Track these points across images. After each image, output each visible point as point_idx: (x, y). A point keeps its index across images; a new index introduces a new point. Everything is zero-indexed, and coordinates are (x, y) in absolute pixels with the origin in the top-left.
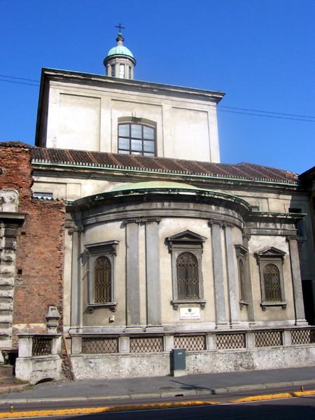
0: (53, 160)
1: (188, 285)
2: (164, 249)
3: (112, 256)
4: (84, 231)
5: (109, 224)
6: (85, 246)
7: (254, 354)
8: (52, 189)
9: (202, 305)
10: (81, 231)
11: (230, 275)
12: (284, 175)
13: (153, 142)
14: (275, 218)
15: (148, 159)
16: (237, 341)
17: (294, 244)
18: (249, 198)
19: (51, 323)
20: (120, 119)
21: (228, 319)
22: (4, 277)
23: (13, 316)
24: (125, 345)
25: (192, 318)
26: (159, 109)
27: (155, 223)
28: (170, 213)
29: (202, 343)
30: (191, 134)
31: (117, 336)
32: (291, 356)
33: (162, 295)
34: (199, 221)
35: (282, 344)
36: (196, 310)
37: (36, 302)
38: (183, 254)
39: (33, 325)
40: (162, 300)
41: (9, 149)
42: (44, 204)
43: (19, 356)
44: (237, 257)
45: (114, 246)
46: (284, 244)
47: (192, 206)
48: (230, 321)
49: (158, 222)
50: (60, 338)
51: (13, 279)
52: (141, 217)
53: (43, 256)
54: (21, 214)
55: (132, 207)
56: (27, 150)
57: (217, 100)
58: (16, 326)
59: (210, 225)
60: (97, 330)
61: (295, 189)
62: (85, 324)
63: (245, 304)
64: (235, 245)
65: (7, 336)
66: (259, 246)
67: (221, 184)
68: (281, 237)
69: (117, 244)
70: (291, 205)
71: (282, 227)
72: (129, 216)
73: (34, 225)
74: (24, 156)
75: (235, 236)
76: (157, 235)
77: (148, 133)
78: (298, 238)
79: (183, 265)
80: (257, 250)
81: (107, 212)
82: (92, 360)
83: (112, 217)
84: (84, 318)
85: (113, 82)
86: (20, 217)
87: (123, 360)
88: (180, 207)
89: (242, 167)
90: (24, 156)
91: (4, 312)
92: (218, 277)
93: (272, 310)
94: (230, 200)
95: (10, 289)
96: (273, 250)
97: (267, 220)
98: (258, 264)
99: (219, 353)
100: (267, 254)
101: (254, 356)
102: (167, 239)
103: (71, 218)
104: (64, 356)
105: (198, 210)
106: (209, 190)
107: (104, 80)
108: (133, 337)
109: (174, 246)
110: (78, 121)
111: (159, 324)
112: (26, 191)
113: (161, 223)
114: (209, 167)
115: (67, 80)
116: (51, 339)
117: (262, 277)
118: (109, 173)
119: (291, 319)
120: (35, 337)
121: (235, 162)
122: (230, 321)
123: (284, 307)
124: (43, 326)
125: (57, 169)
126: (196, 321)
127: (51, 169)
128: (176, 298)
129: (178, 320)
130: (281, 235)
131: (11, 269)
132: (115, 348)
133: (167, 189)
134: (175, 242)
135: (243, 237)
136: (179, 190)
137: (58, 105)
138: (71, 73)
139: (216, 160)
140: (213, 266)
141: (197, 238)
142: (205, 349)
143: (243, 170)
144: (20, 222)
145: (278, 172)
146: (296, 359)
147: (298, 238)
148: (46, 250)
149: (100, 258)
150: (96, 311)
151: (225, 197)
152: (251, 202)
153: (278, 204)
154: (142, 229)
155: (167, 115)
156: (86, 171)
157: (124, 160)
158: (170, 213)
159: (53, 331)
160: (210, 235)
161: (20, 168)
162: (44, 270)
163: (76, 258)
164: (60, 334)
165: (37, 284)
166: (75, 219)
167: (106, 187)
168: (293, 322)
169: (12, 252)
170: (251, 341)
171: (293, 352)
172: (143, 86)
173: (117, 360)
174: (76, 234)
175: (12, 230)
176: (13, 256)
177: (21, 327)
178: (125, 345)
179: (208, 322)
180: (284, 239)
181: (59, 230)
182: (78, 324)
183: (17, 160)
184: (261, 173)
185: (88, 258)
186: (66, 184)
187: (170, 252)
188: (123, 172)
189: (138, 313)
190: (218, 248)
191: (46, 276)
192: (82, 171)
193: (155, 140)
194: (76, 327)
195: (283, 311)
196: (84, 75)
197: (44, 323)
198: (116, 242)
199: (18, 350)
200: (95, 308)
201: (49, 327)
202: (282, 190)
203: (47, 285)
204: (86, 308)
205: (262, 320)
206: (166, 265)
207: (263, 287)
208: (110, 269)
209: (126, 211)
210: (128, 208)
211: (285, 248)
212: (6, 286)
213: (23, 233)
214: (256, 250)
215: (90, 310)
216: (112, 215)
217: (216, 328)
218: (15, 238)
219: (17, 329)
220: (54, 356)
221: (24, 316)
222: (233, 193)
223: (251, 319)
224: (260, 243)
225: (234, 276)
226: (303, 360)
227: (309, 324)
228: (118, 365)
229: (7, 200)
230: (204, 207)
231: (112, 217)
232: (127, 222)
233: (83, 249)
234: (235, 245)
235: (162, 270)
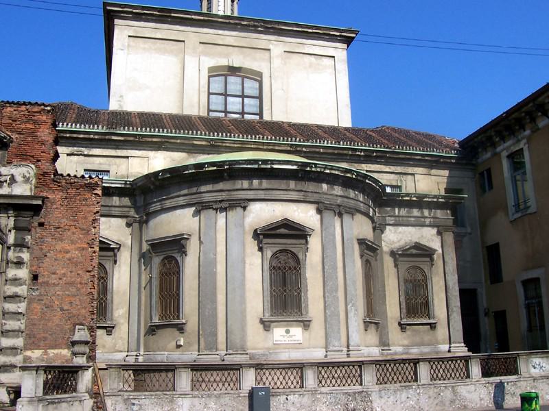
0: (110, 124)
1: (286, 295)
2: (252, 245)
3: (182, 255)
4: (147, 222)
5: (179, 212)
6: (147, 241)
7: (373, 394)
8: (110, 165)
9: (306, 325)
10: (143, 222)
11: (348, 282)
12: (440, 143)
13: (258, 100)
14: (420, 202)
15: (218, 119)
16: (354, 376)
17: (449, 238)
18: (385, 176)
19: (77, 348)
20: (211, 70)
21: (346, 344)
22: (11, 285)
23: (25, 339)
24: (184, 380)
25: (288, 341)
26: (267, 53)
27: (239, 210)
28: (261, 194)
29: (298, 378)
30: (311, 87)
31: (173, 368)
32: (430, 397)
33: (248, 310)
34: (303, 206)
35: (416, 380)
36: (297, 332)
37: (57, 319)
38: (281, 251)
39: (52, 352)
40: (249, 318)
41: (23, 108)
42: (71, 183)
43: (22, 395)
44: (362, 256)
45: (183, 241)
47: (292, 184)
48: (348, 347)
49: (244, 208)
50: (91, 369)
51: (25, 287)
52: (221, 201)
53: (68, 256)
55: (209, 187)
56: (49, 108)
57: (348, 41)
58: (29, 353)
59: (319, 211)
60: (163, 356)
61: (453, 161)
62: (147, 350)
63: (373, 320)
64: (358, 240)
65: (15, 367)
66: (399, 241)
67: (346, 155)
68: (430, 228)
69: (187, 239)
70: (447, 183)
71: (432, 215)
72: (206, 199)
73: (56, 213)
74: (44, 118)
75: (360, 227)
76: (242, 226)
77: (251, 87)
78: (456, 230)
79: (279, 268)
80: (396, 246)
81: (175, 194)
82: (136, 402)
83: (182, 201)
84: (145, 340)
86: (35, 202)
87: (180, 401)
88: (275, 187)
89: (381, 132)
90: (44, 118)
91: (11, 333)
92: (330, 283)
93: (414, 330)
94: (349, 175)
95: (20, 302)
96: (417, 246)
97: (410, 205)
98: (396, 266)
99: (321, 393)
100: (408, 252)
101: (374, 397)
102: (256, 230)
103: (129, 204)
104: (96, 395)
105: (302, 191)
106: (327, 165)
108: (196, 368)
109: (265, 241)
110: (153, 73)
112: (46, 166)
113: (248, 208)
114: (334, 132)
115: (138, 17)
116: (77, 372)
117: (402, 283)
118: (186, 142)
120: (47, 369)
121: (373, 126)
122: (348, 347)
123: (433, 326)
124: (66, 352)
125: (114, 138)
126: (298, 346)
127: (107, 137)
128: (267, 315)
129: (270, 344)
130: (430, 226)
131: (23, 273)
133: (256, 162)
134: (266, 236)
135: (374, 229)
136: (273, 162)
137: (126, 51)
138: (143, 8)
139: (346, 122)
140: (323, 268)
141: (300, 230)
142: (302, 387)
143: (381, 136)
144: (36, 210)
145: (428, 136)
146: (436, 401)
147: (456, 230)
148: (73, 246)
149: (165, 258)
150: (160, 332)
151: (342, 172)
152: (384, 179)
153: (427, 182)
154: (221, 218)
155: (277, 62)
156: (155, 140)
157: (211, 124)
158: (261, 194)
159: (80, 361)
160: (319, 225)
163: (136, 257)
164: (91, 364)
165: (58, 295)
166: (135, 206)
167: (183, 159)
168: (446, 347)
169: (25, 250)
170: (369, 376)
171: (432, 392)
172: (242, 23)
173: (172, 401)
174: (136, 225)
175: (24, 221)
176: (25, 256)
177: (35, 354)
178: (184, 380)
179: (314, 348)
180: (434, 231)
181: (91, 219)
182: (138, 349)
183: (35, 122)
184: (405, 140)
185: (151, 258)
186: (128, 157)
187: (261, 249)
188: (206, 140)
189: (215, 335)
190: (332, 244)
191: (72, 284)
192: (150, 140)
193: (260, 97)
194: (135, 353)
195: (432, 332)
197: (68, 348)
198: (185, 236)
199: (21, 388)
200: (159, 327)
201: (74, 354)
202: (433, 163)
203: (74, 296)
204: (148, 327)
205: (400, 345)
206: (255, 269)
208: (178, 273)
210: (203, 188)
212: (14, 298)
213: (41, 224)
214: (393, 246)
215: (153, 330)
216: (181, 198)
217: (326, 356)
218: (30, 231)
219: (30, 358)
220: (79, 395)
221: (40, 340)
222: (364, 168)
223: (384, 343)
225: (354, 283)
226: (447, 403)
227: (469, 351)
229: (19, 178)
230: (311, 187)
231: (182, 201)
232: (202, 208)
233: (145, 247)
234: (358, 240)
235: (248, 275)
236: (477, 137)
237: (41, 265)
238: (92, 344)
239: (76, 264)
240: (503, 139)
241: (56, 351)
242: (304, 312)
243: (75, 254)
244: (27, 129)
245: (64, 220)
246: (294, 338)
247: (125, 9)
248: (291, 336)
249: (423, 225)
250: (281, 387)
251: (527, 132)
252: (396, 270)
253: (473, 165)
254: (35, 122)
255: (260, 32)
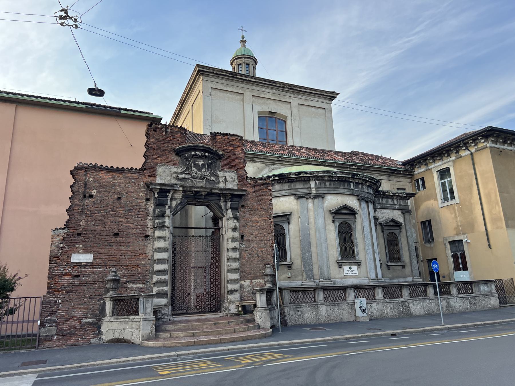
9: (359, 264)
24: (320, 296)
26: (289, 106)
31: (344, 288)
36: (355, 268)
41: (226, 137)
46: (400, 216)
53: (259, 224)
54: (243, 191)
58: (242, 282)
66: (382, 218)
68: (397, 211)
74: (238, 144)
85: (254, 80)
96: (393, 221)
97: (388, 197)
98: (383, 232)
101: (411, 305)
107: (247, 79)
111: (329, 279)
119: (409, 277)
123: (403, 267)
126: (356, 277)
129: (342, 275)
132: (313, 300)
144: (240, 196)
155: (295, 111)
161: (236, 153)
162: (260, 235)
173: (317, 309)
181: (268, 203)
183: (233, 146)
187: (333, 221)
191: (262, 241)
195: (403, 270)
196: (236, 78)
207: (387, 251)
209: (297, 189)
211: (401, 220)
219: (243, 285)
224: (383, 215)
228: (318, 313)
232: (298, 197)
236: (417, 160)
237: (245, 230)
238: (273, 276)
239: (263, 229)
240: (434, 161)
241: (257, 281)
242: (357, 257)
243: (262, 223)
244: (229, 149)
245: (255, 204)
246: (354, 272)
247: (209, 71)
248: (352, 271)
249: (395, 209)
250: (309, 301)
251: (453, 158)
252: (382, 234)
253: (411, 175)
254: (233, 146)
255: (286, 91)
